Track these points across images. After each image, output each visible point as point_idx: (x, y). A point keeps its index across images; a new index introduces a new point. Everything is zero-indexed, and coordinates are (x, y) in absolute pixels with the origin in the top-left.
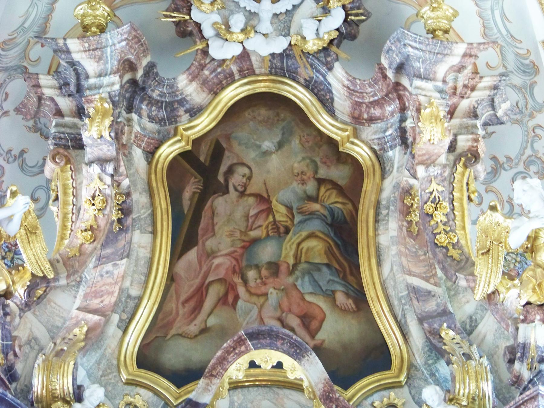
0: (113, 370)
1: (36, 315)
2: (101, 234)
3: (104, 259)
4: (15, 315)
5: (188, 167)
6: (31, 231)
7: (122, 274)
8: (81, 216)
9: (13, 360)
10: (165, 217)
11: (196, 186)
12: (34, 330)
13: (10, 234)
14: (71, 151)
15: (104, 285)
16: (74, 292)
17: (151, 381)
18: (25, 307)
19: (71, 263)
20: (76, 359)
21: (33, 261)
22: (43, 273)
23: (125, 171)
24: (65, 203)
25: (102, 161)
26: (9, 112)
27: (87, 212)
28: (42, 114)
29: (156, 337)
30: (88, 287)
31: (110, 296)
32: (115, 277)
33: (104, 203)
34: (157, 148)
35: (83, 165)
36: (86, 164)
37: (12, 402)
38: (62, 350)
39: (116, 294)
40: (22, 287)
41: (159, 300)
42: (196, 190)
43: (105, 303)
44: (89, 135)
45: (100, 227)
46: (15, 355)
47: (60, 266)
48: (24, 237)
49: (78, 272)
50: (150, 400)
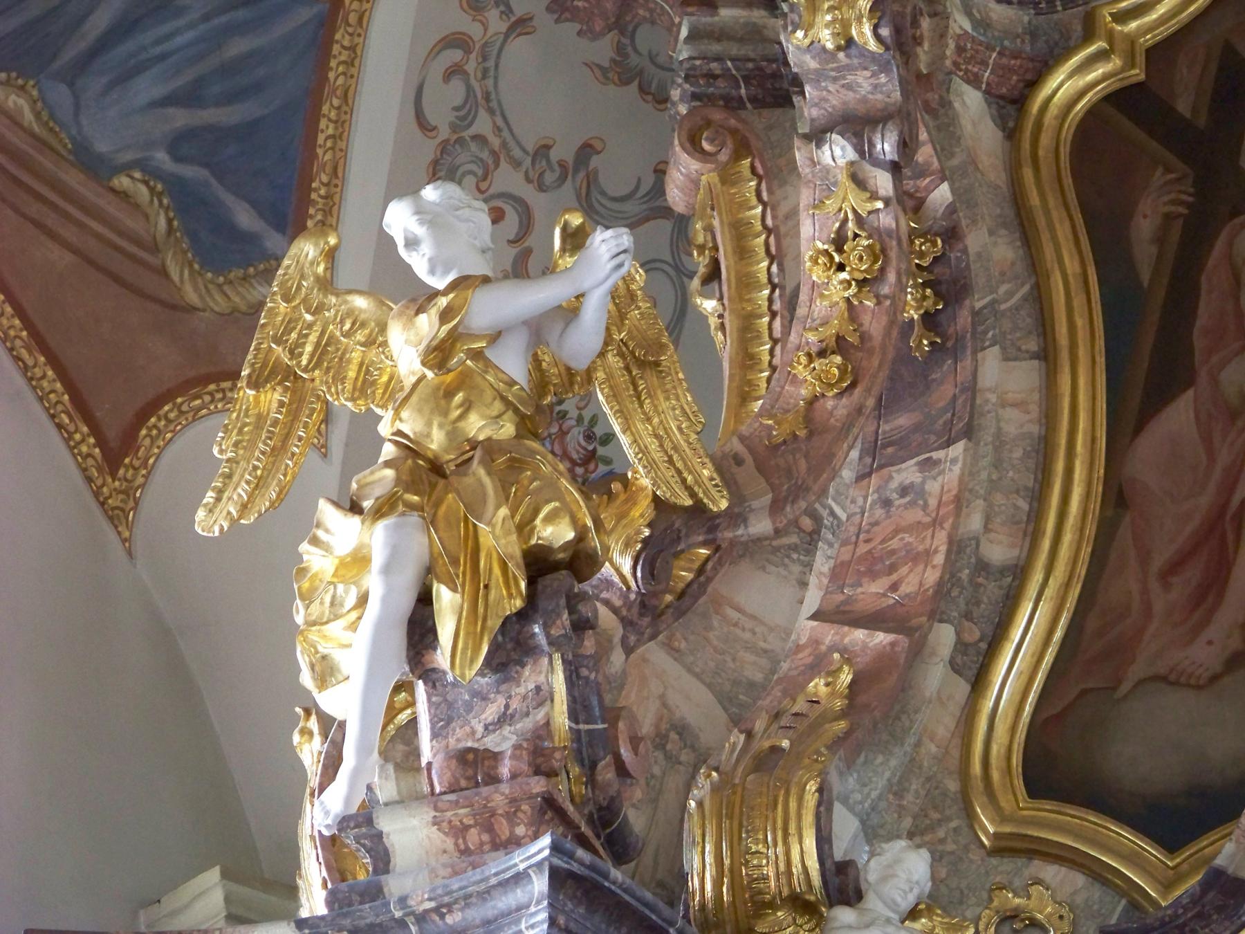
0: (948, 812)
1: (677, 651)
2: (876, 363)
3: (890, 450)
4: (610, 641)
5: (1140, 135)
6: (641, 361)
7: (954, 492)
8: (801, 311)
9: (616, 786)
10: (1079, 301)
11: (1173, 196)
12: (674, 699)
13: (573, 364)
14: (749, 113)
15: (897, 532)
16: (796, 569)
17: (1078, 836)
18: (641, 615)
19: (781, 462)
20: (823, 774)
21: (658, 456)
22: (693, 495)
23: (935, 160)
24: (746, 284)
25: (857, 125)
26: (531, 19)
27: (822, 296)
28: (641, 12)
29: (1084, 693)
30: (845, 543)
31: (921, 567)
32: (933, 502)
33: (875, 262)
34: (1034, 83)
35: (797, 142)
36: (807, 138)
37: (627, 898)
38: (775, 749)
39: (939, 559)
40: (627, 545)
41: (1082, 570)
42: (1173, 208)
43: (906, 589)
44: (807, 41)
45: (870, 338)
46: (622, 771)
47: (747, 473)
48: (622, 379)
49: (808, 489)
50: (1079, 900)
